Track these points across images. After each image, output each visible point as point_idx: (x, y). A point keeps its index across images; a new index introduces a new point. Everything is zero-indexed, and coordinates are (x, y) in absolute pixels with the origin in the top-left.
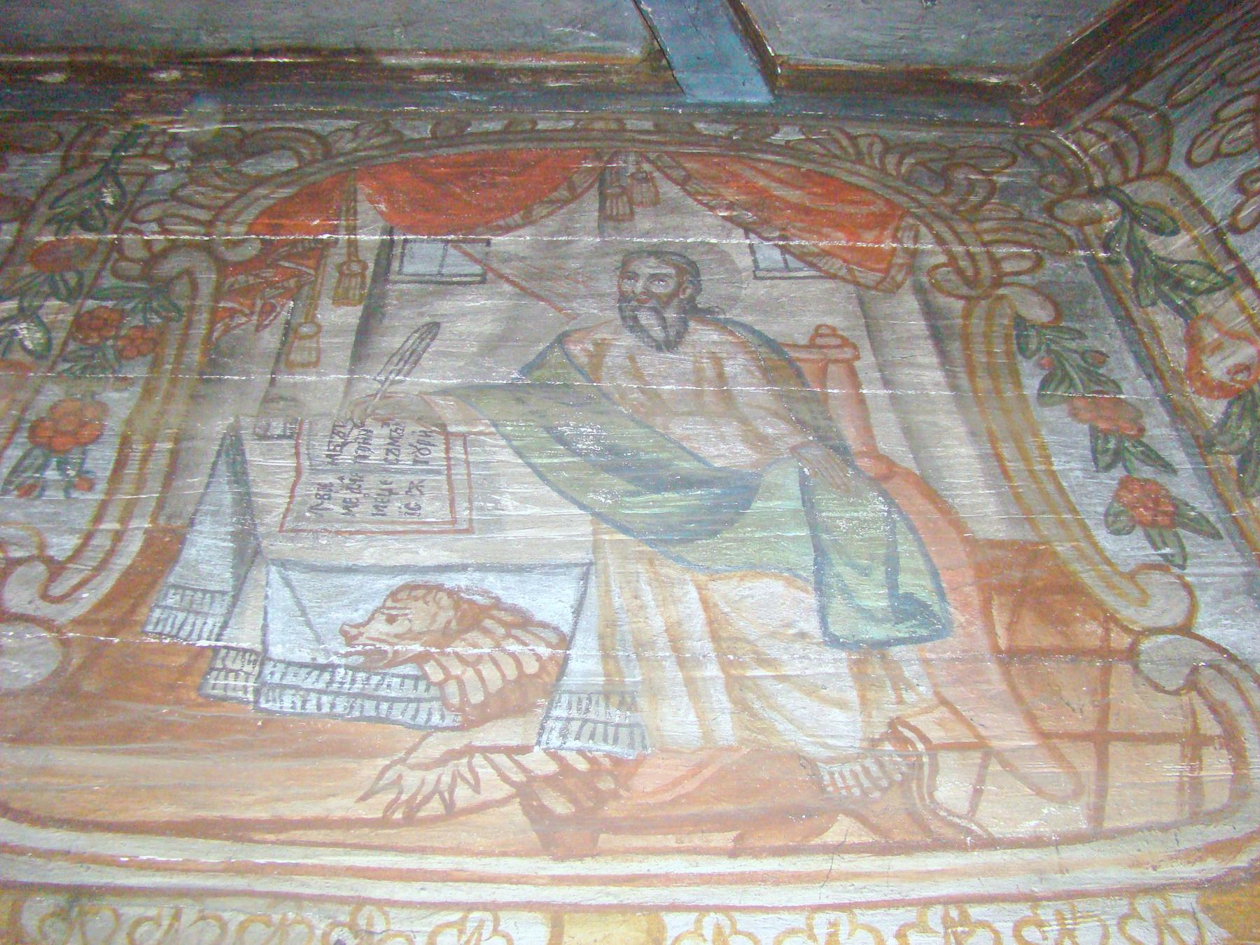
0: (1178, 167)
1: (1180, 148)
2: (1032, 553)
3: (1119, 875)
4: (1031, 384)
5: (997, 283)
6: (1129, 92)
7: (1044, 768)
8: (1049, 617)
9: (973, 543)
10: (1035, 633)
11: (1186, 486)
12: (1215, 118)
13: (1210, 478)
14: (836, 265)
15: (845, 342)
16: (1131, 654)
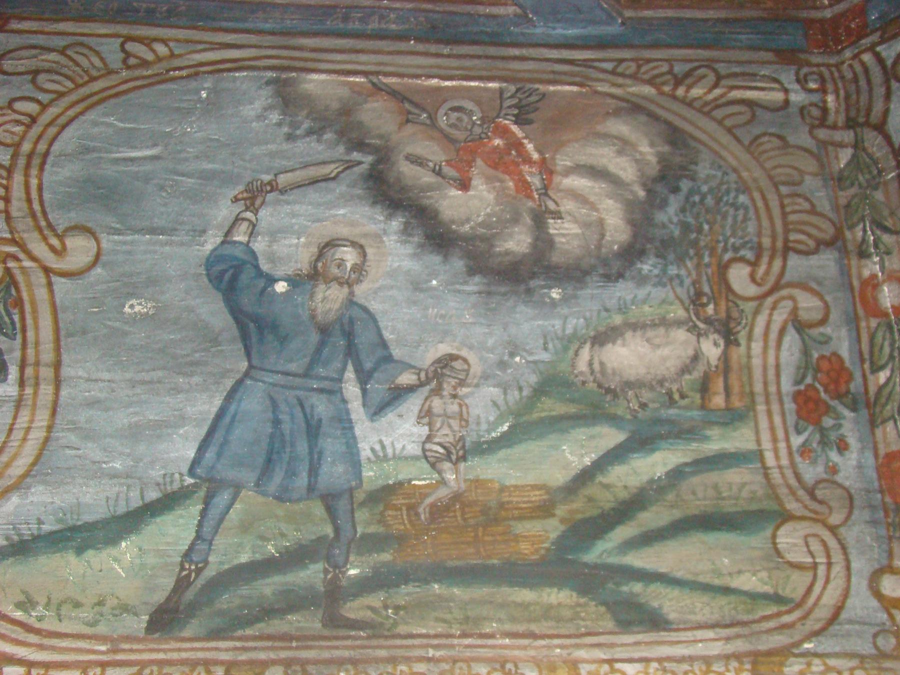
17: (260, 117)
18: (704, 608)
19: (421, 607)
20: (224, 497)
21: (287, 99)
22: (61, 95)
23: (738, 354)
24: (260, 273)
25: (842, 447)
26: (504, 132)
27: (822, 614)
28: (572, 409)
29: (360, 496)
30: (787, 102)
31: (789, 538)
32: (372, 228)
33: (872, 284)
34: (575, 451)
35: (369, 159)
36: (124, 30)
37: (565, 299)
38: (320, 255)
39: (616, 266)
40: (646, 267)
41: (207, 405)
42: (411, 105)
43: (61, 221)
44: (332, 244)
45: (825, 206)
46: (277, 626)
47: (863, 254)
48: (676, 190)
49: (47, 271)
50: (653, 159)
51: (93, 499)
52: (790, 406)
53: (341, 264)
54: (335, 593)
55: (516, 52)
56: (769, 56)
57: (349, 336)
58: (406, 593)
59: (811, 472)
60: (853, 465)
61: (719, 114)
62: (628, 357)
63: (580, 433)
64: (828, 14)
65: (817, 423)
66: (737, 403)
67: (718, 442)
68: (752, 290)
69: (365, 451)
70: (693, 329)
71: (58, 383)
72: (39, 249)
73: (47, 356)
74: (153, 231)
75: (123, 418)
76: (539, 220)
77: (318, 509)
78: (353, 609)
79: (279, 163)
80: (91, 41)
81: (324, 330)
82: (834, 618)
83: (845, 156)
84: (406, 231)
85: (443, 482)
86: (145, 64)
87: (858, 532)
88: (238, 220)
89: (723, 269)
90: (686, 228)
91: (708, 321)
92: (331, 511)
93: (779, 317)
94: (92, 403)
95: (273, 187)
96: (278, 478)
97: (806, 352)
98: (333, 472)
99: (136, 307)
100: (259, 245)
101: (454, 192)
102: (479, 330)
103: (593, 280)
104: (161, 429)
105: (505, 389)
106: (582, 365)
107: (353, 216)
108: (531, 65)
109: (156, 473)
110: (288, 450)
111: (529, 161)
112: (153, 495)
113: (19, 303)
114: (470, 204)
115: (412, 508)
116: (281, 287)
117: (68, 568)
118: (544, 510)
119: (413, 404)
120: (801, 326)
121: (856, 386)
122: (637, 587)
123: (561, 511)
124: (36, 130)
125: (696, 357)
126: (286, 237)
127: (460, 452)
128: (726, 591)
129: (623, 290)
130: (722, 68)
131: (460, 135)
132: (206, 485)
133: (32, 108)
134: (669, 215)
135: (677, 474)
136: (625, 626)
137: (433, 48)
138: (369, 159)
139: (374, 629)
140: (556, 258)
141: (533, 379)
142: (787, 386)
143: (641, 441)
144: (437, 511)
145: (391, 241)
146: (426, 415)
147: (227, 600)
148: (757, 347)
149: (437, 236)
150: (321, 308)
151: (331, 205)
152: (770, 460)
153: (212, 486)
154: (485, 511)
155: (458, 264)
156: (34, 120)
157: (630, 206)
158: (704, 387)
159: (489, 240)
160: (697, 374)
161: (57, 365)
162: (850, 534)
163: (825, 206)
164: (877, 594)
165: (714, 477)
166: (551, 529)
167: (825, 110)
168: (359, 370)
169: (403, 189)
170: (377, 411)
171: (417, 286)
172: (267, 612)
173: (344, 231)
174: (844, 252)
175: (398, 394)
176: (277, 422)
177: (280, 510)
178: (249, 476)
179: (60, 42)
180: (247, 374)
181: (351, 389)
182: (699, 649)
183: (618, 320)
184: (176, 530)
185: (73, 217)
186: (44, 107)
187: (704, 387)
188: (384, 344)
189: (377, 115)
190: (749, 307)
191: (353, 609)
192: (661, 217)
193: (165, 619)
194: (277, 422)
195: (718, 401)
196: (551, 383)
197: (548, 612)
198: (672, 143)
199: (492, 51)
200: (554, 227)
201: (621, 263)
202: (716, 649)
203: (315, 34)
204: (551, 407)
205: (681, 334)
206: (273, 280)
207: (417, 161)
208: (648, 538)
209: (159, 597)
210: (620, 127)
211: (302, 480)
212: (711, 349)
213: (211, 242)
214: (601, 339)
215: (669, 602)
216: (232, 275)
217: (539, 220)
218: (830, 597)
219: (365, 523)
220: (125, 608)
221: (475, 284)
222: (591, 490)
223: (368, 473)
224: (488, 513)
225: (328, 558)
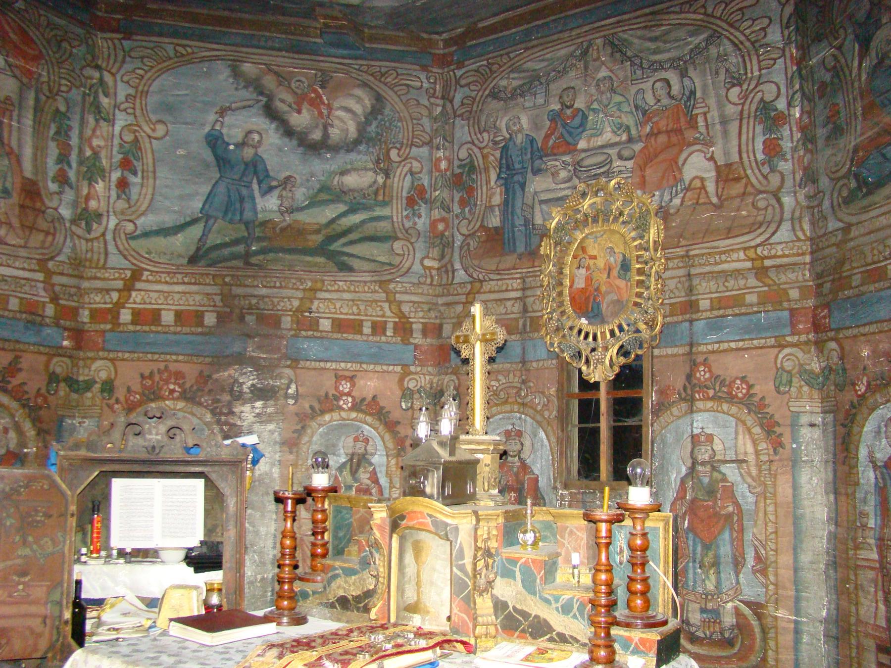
0: (118, 77)
1: (122, 71)
2: (34, 183)
3: (26, 255)
4: (52, 132)
5: (57, 94)
6: (124, 39)
7: (20, 232)
8: (32, 199)
9: (23, 177)
10: (28, 203)
11: (72, 175)
12: (134, 71)
13: (78, 172)
14: (17, 73)
15: (12, 105)
16: (44, 212)
17: (226, 80)
18: (366, 266)
19: (275, 261)
20: (211, 222)
21: (236, 73)
22: (152, 67)
23: (389, 182)
24: (224, 142)
25: (420, 216)
26: (315, 91)
27: (404, 270)
28: (330, 198)
29: (257, 223)
30: (421, 87)
31: (397, 245)
32: (264, 126)
33: (439, 160)
34: (329, 212)
35: (265, 99)
36: (175, 41)
37: (332, 158)
38: (246, 136)
39: (351, 146)
40: (362, 148)
41: (206, 189)
42: (283, 79)
43: (154, 118)
44: (250, 132)
45: (428, 129)
46: (229, 264)
47: (438, 149)
48: (376, 119)
49: (149, 137)
50: (369, 106)
51: (169, 220)
52: (404, 201)
53: (253, 140)
54: (248, 255)
55: (322, 58)
56: (417, 67)
57: (255, 166)
58: (271, 256)
59: (408, 224)
60: (422, 223)
61: (396, 89)
62: (351, 180)
63: (332, 206)
64: (441, 52)
65: (413, 207)
66: (387, 199)
67: (378, 212)
68: (398, 159)
69: (259, 207)
70: (375, 172)
71: (155, 178)
72: (146, 128)
73: (151, 169)
74: (186, 123)
75: (177, 192)
76: (325, 128)
77: (243, 227)
78: (253, 260)
79: (232, 99)
80: (164, 45)
81: (246, 164)
82: (407, 272)
83: (439, 109)
84: (277, 129)
85: (285, 220)
86: (183, 55)
87: (420, 245)
88: (217, 121)
89: (388, 151)
90: (378, 133)
91: (381, 169)
92: (247, 229)
93: (406, 169)
94: (166, 186)
95: (230, 108)
96: (230, 215)
97: (413, 183)
98: (248, 215)
99: (181, 152)
100: (224, 131)
101: (295, 115)
102: (300, 167)
103: (342, 151)
104: (190, 196)
105: (308, 189)
106: (335, 182)
107: (258, 121)
108: (327, 65)
109: (189, 212)
110: (234, 205)
111: (324, 103)
112: (188, 219)
113: (140, 149)
114: (301, 119)
115: (274, 228)
116: (232, 147)
117: (161, 242)
118: (318, 232)
119: (276, 193)
120: (412, 173)
121: (427, 196)
122: (346, 258)
123: (323, 232)
124: (144, 81)
125: (375, 182)
126: (234, 128)
127: (291, 210)
128: (374, 261)
129: (353, 156)
130: (399, 71)
131: (299, 92)
132: (206, 217)
133: (141, 72)
134: (372, 128)
135: (363, 222)
136: (341, 270)
137: (291, 55)
138: (265, 99)
139: (260, 267)
140: (330, 142)
141: (318, 186)
142: (405, 194)
143: (352, 210)
144: (283, 230)
145: (272, 132)
146: (280, 197)
147: (214, 255)
148: (396, 179)
149: (289, 132)
150: (245, 156)
151: (250, 117)
152: (395, 219)
153: (208, 217)
154: (298, 230)
155: (295, 142)
156: (143, 77)
157: (359, 124)
158: (376, 193)
159: (306, 134)
160: (374, 188)
161: (154, 172)
162: (417, 245)
163: (428, 129)
164: (422, 264)
165: (375, 224)
166: (319, 238)
167: (435, 90)
168: (258, 178)
169: (277, 112)
170: (264, 194)
171: (280, 149)
172: (225, 260)
173: (255, 128)
174: (432, 148)
175: (271, 189)
176: (229, 197)
177: (230, 226)
178: (220, 215)
179: (151, 45)
180: (220, 178)
181: (255, 186)
182: (363, 279)
183: (349, 167)
184: (196, 231)
185: (158, 117)
186: (146, 72)
187: (376, 193)
188: (267, 171)
189: (269, 82)
190: (395, 165)
191: (253, 260)
192: (369, 129)
193: (193, 260)
194: (229, 197)
195: (380, 198)
196: (324, 188)
197: (316, 265)
198: (377, 100)
199: (314, 57)
200: (331, 130)
201: (351, 146)
202: (369, 279)
203: (247, 46)
204: (324, 196)
205: (371, 173)
206: (228, 144)
207: (283, 101)
208: (352, 243)
209: (191, 253)
210: (359, 92)
211: (238, 217)
212: (380, 180)
213: (207, 129)
214: (343, 173)
215: (355, 263)
216: (214, 141)
217: (325, 128)
218: (407, 265)
219: (258, 232)
220: (180, 256)
221: (301, 150)
222: (334, 226)
223: (260, 216)
224: (300, 231)
225: (246, 243)
